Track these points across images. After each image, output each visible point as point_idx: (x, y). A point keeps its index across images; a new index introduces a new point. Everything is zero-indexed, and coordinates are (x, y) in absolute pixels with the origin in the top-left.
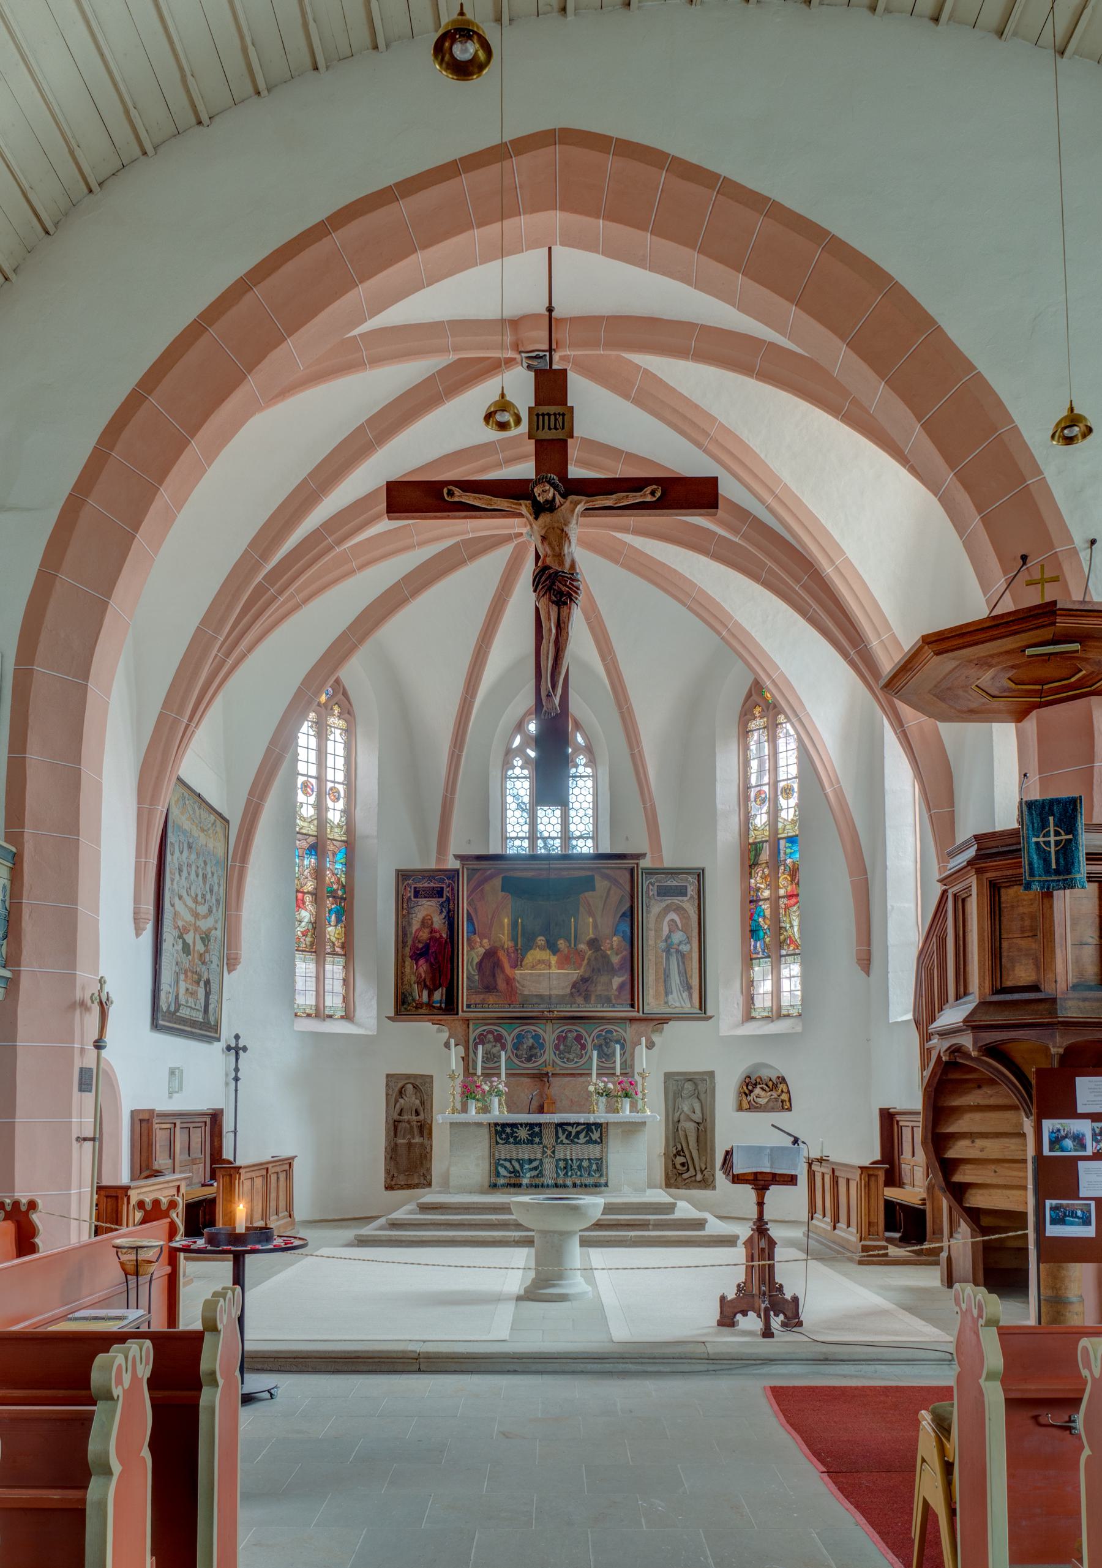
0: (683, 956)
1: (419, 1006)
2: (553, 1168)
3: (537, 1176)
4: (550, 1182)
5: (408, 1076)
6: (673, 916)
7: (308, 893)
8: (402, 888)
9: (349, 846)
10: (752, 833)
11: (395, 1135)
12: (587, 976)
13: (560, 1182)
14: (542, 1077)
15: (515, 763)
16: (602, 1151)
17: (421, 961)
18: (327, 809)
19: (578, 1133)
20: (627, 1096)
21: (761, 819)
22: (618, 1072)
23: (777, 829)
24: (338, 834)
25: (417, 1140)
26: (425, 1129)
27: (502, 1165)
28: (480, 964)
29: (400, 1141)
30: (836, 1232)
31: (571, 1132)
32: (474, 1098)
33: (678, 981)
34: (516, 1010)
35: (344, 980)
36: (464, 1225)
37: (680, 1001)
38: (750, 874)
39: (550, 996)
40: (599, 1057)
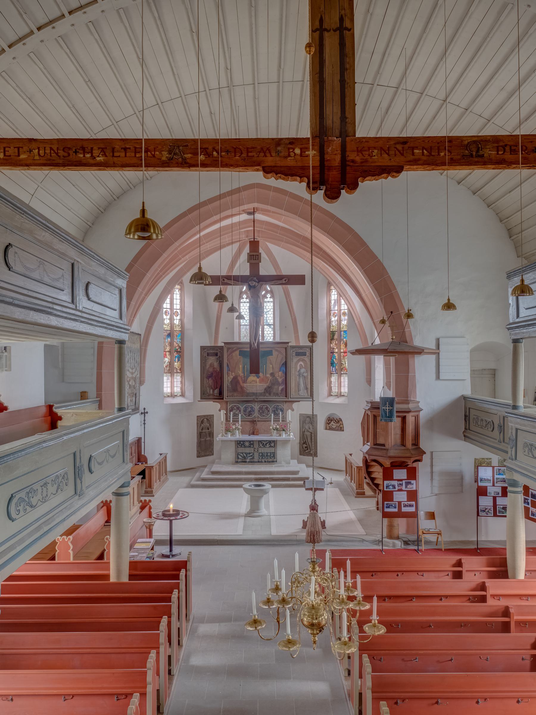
0: (305, 377)
1: (209, 395)
5: (204, 416)
6: (301, 363)
8: (203, 353)
9: (182, 332)
10: (332, 327)
13: (260, 460)
14: (253, 422)
17: (210, 379)
18: (174, 320)
19: (266, 444)
20: (284, 430)
24: (178, 329)
26: (211, 434)
28: (231, 381)
37: (303, 393)
39: (257, 393)
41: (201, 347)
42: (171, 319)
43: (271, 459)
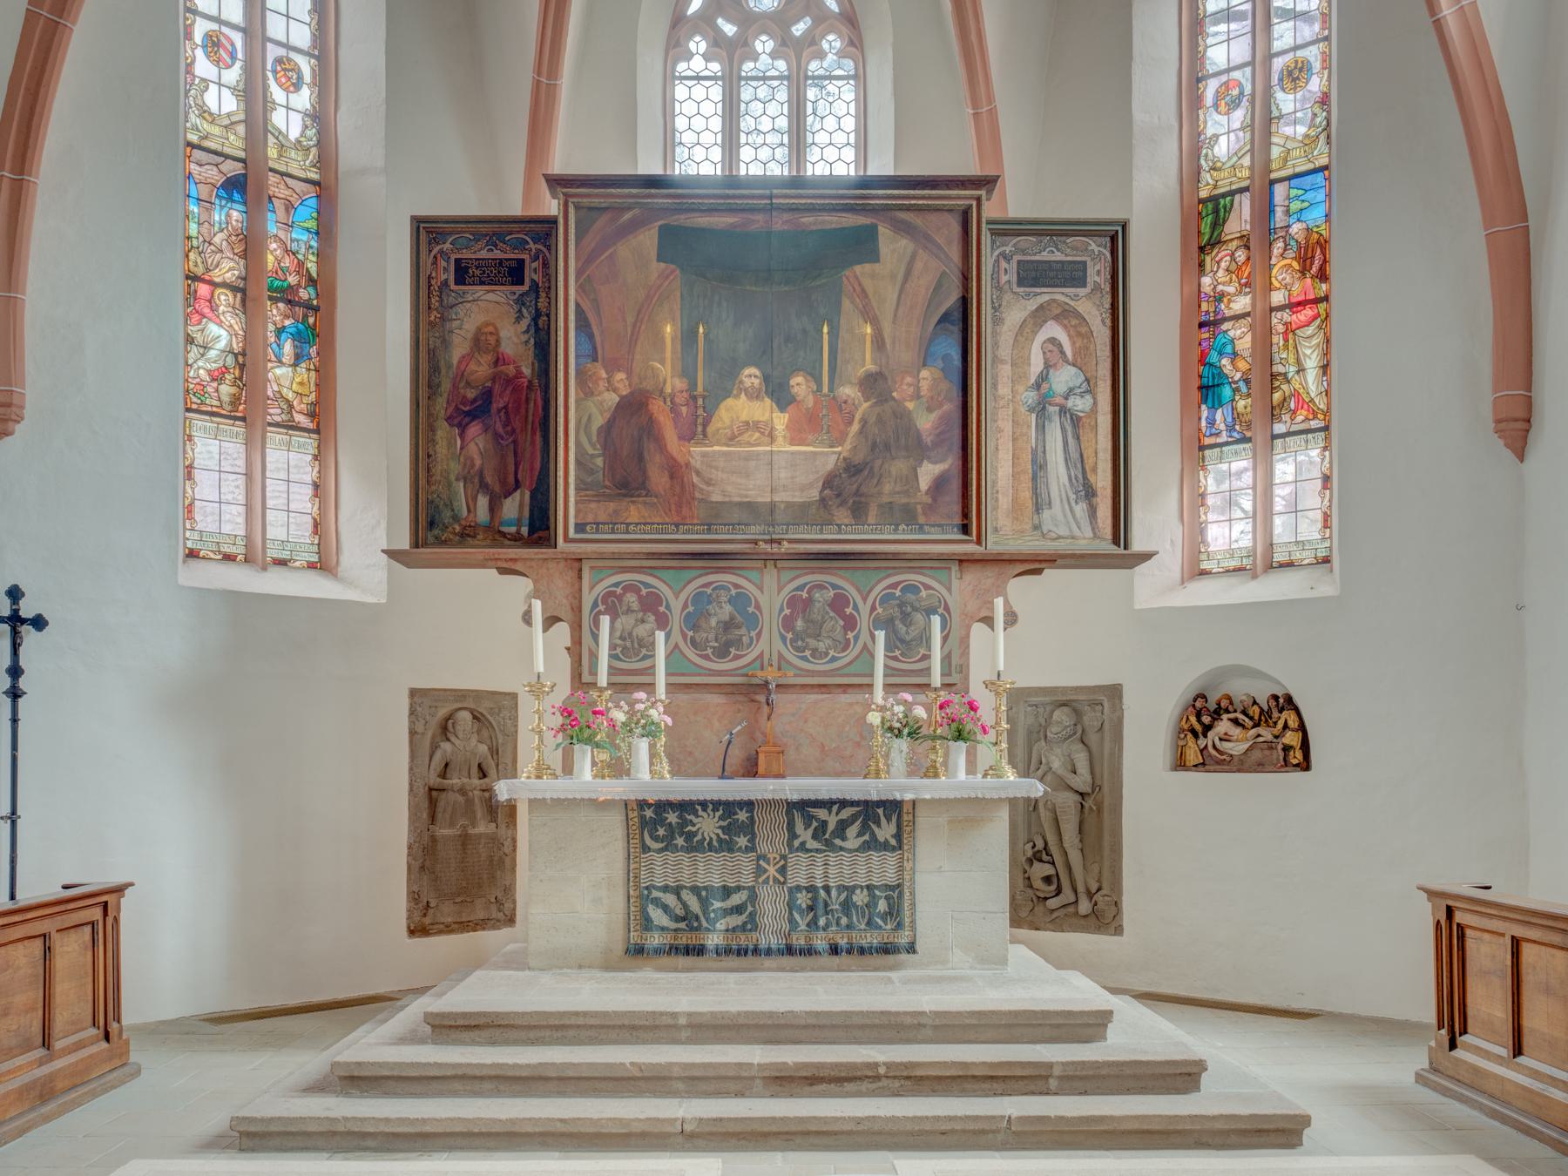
0: (1076, 421)
2: (782, 907)
3: (743, 928)
4: (775, 942)
6: (1053, 330)
7: (224, 285)
8: (426, 268)
9: (324, 190)
10: (1206, 177)
11: (433, 818)
12: (858, 459)
13: (799, 941)
15: (692, 46)
16: (901, 869)
17: (474, 429)
19: (842, 826)
20: (960, 736)
21: (1225, 136)
22: (936, 680)
23: (1268, 161)
24: (300, 165)
25: (483, 828)
27: (656, 902)
28: (607, 430)
29: (443, 832)
30: (1455, 1053)
31: (824, 824)
32: (589, 741)
33: (1064, 479)
34: (693, 538)
35: (316, 486)
36: (547, 1079)
37: (1070, 523)
38: (1201, 265)
39: (772, 507)
40: (889, 647)
41: (414, 218)
42: (252, 95)
43: (875, 931)
